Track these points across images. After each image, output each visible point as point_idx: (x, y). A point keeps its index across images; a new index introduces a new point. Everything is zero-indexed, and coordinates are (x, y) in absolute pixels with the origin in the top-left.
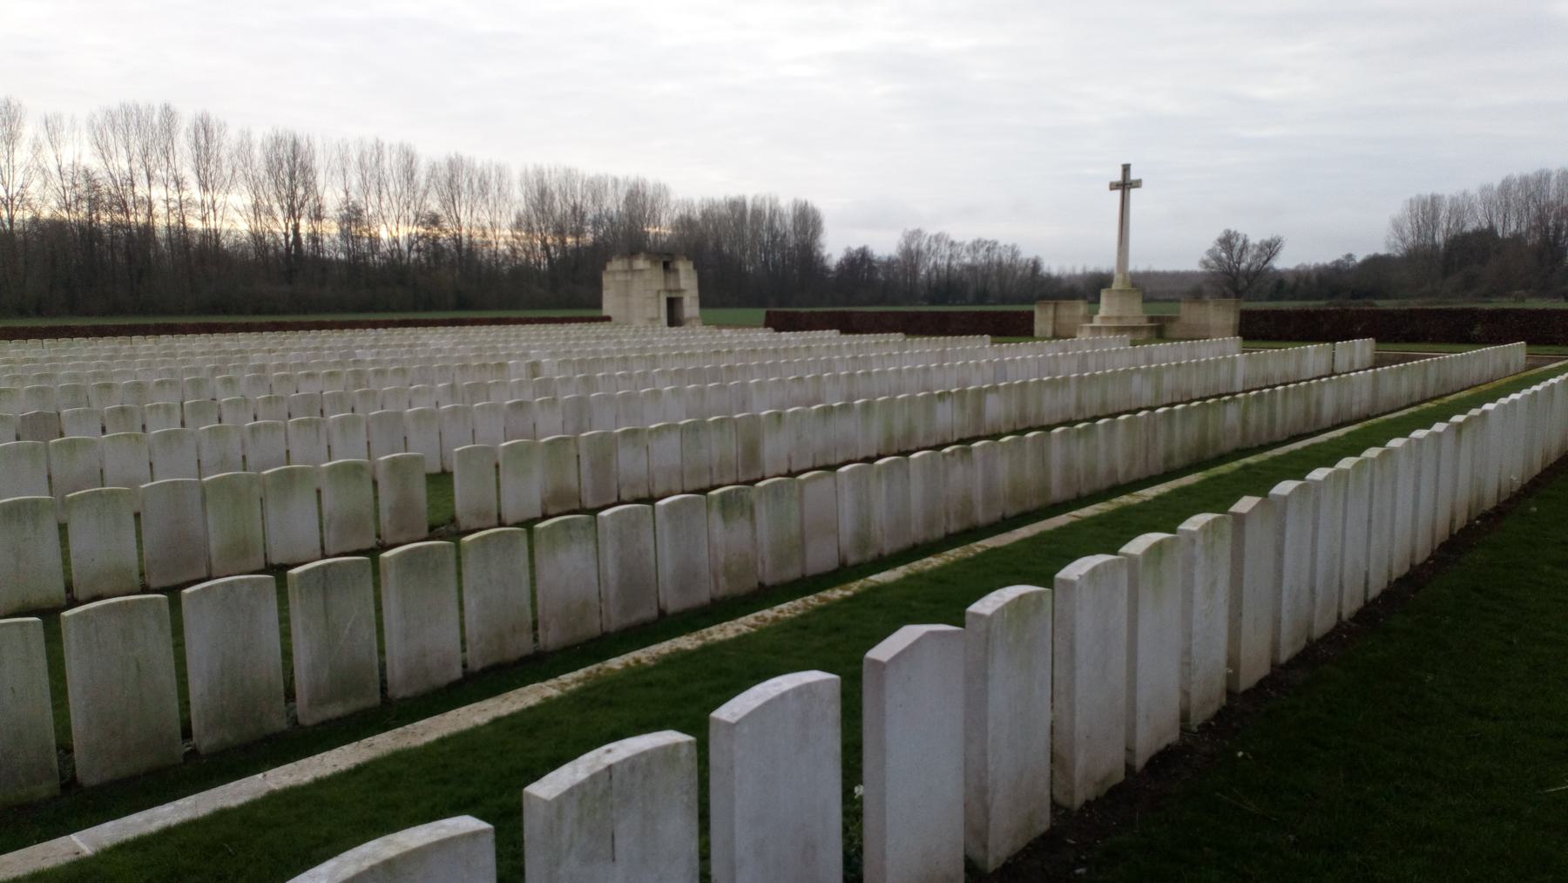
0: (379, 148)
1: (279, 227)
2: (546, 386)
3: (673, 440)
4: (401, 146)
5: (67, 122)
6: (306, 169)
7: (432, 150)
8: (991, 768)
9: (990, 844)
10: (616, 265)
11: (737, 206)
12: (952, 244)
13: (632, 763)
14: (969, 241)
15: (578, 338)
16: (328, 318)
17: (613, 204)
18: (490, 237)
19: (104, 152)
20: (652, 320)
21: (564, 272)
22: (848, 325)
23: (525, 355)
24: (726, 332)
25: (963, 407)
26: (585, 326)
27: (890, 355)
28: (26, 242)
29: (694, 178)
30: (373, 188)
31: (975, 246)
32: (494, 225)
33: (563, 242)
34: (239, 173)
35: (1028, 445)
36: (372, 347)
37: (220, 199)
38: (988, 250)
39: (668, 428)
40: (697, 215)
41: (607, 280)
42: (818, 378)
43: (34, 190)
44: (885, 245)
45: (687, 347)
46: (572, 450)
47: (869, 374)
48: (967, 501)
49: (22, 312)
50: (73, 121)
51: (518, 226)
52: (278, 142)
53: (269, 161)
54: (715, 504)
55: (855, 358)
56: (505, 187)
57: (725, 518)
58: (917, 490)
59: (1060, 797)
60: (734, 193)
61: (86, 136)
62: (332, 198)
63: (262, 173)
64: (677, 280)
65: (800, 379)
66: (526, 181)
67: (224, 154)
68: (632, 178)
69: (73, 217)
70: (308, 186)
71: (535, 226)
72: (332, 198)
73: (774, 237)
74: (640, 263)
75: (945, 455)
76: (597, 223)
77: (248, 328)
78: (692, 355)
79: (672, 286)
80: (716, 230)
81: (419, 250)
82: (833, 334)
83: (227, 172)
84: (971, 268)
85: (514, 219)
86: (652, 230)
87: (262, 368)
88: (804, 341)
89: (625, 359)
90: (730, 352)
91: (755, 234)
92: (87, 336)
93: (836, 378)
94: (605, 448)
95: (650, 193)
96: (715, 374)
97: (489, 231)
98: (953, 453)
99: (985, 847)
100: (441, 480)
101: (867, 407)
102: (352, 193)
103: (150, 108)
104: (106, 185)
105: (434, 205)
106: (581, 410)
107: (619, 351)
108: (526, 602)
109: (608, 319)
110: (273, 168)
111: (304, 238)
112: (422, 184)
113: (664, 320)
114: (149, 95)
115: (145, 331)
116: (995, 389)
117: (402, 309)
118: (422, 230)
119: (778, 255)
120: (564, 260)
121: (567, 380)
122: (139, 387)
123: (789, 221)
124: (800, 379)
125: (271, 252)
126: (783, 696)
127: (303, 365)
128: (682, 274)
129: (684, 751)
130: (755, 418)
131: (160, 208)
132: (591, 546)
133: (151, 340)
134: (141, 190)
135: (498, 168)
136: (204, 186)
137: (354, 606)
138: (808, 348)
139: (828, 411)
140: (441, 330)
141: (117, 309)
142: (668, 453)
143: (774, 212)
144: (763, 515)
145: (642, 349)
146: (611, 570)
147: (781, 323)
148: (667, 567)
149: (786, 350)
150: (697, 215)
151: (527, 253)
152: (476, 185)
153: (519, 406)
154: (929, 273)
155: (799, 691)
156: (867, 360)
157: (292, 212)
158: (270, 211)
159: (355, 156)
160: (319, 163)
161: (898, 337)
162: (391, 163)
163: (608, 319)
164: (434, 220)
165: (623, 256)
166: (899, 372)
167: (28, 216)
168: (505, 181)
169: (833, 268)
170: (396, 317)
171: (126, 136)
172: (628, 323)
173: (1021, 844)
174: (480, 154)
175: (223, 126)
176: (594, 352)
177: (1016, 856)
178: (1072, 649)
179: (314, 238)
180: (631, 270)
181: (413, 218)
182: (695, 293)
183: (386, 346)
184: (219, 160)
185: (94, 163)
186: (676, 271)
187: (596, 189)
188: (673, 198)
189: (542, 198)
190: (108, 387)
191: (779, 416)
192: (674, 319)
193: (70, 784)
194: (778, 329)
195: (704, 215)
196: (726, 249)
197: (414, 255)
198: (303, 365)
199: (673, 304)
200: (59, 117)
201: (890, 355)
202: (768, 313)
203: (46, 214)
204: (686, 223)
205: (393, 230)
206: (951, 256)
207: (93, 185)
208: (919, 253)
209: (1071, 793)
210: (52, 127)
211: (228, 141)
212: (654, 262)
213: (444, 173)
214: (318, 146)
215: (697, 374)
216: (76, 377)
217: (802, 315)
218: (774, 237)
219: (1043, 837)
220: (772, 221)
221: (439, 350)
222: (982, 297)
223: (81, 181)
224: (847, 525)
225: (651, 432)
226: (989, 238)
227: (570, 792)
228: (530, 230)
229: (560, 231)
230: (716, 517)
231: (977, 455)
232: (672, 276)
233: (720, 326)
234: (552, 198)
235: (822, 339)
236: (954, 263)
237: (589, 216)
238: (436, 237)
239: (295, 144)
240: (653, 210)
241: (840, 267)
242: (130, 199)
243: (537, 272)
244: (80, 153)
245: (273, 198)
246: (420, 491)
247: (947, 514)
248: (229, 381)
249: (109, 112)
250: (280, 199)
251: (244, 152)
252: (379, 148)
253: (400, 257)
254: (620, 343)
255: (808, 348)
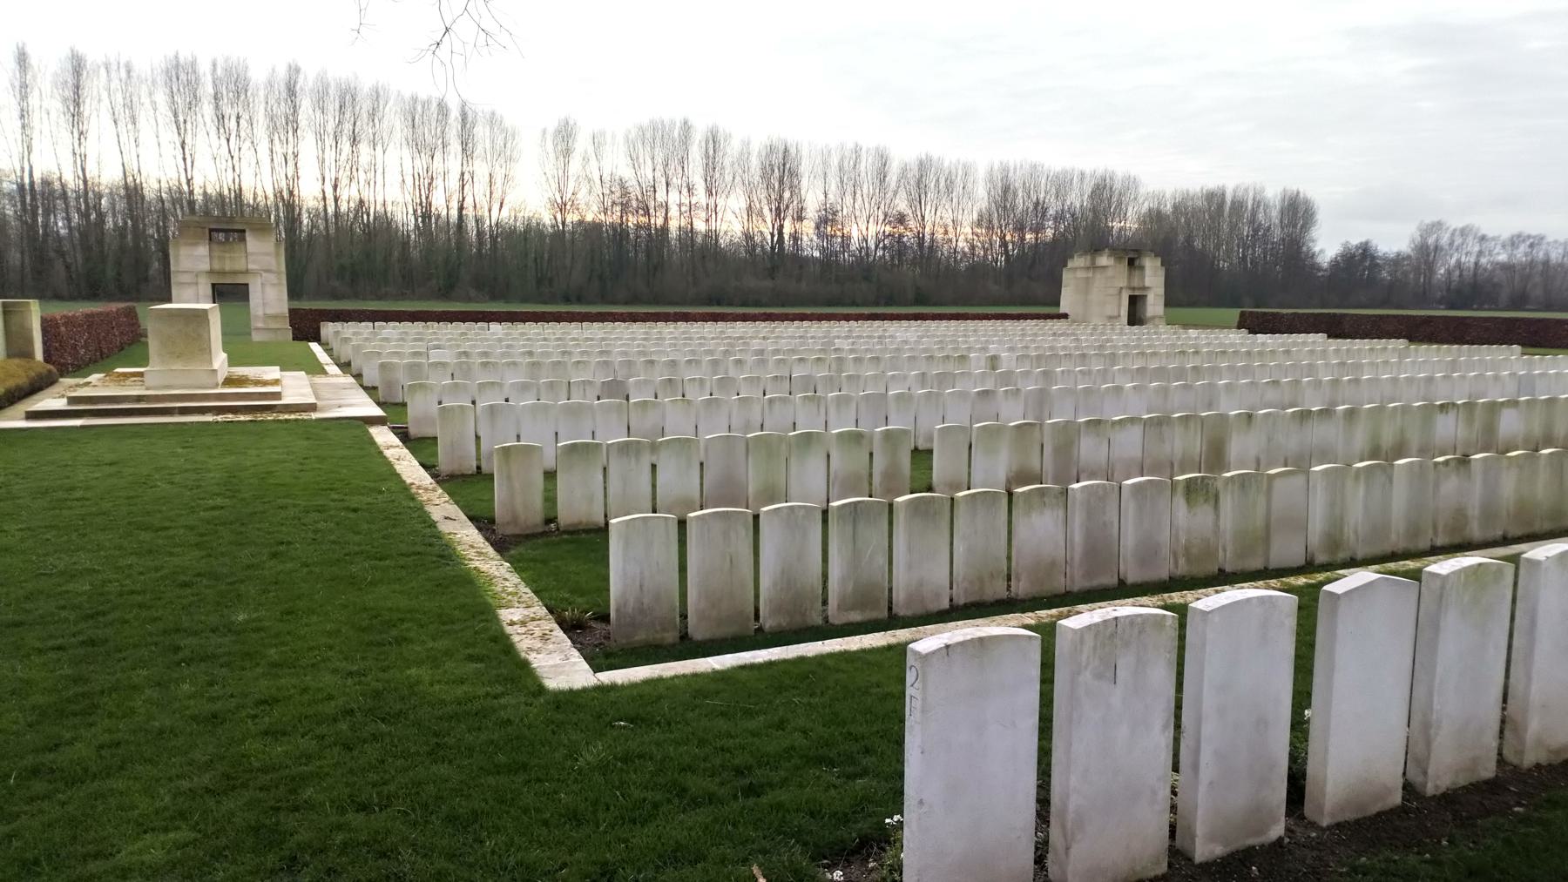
0: (857, 151)
1: (764, 228)
2: (1007, 377)
3: (1136, 432)
4: (877, 149)
5: (609, 139)
6: (793, 174)
7: (904, 154)
8: (1436, 706)
9: (1430, 771)
10: (1078, 262)
11: (1215, 199)
12: (1483, 238)
13: (1132, 619)
14: (1506, 235)
15: (1035, 335)
16: (808, 311)
17: (1077, 199)
18: (951, 235)
19: (634, 161)
20: (1110, 318)
21: (1023, 269)
22: (1336, 328)
23: (985, 349)
24: (1193, 333)
25: (1470, 421)
26: (1041, 322)
27: (1386, 362)
28: (573, 240)
29: (1164, 169)
30: (849, 189)
31: (1514, 242)
32: (957, 225)
33: (1022, 239)
34: (738, 178)
35: (1542, 462)
36: (847, 337)
37: (721, 202)
38: (1531, 246)
39: (1132, 420)
40: (1168, 208)
41: (1067, 276)
42: (1297, 382)
43: (582, 196)
44: (1393, 240)
45: (1149, 346)
46: (1037, 433)
47: (1357, 381)
48: (1460, 515)
49: (567, 300)
50: (613, 137)
51: (979, 223)
52: (772, 149)
53: (764, 168)
54: (1180, 489)
55: (1343, 364)
56: (970, 185)
57: (1188, 501)
58: (1399, 499)
59: (1509, 754)
60: (1211, 183)
61: (623, 148)
62: (813, 203)
63: (757, 178)
64: (1143, 278)
65: (1275, 383)
66: (990, 179)
67: (727, 162)
68: (1100, 171)
69: (609, 220)
70: (794, 189)
71: (995, 222)
72: (813, 203)
73: (1256, 231)
74: (1104, 260)
75: (1436, 464)
76: (1058, 218)
77: (744, 318)
78: (1154, 354)
79: (1136, 283)
80: (1188, 223)
81: (884, 248)
82: (1320, 338)
83: (728, 178)
84: (1507, 268)
85: (975, 216)
86: (1116, 225)
87: (761, 352)
88: (1283, 345)
89: (1084, 356)
90: (1196, 352)
91: (1234, 227)
92: (624, 321)
93: (1318, 384)
94: (1068, 436)
95: (1117, 186)
96: (1180, 373)
97: (950, 229)
98: (1446, 463)
99: (1425, 773)
100: (922, 456)
101: (1351, 414)
102: (830, 196)
103: (673, 123)
104: (635, 192)
105: (902, 205)
106: (1042, 399)
107: (1077, 348)
108: (1004, 555)
109: (1065, 316)
110: (766, 174)
111: (786, 237)
112: (893, 185)
113: (1125, 319)
114: (671, 113)
115: (666, 318)
116: (1514, 403)
117: (865, 304)
118: (888, 229)
119: (1259, 251)
120: (1022, 255)
121: (1026, 374)
122: (673, 363)
123: (1275, 213)
124: (1275, 383)
125: (758, 250)
126: (1249, 600)
127: (793, 351)
128: (1148, 271)
129: (1169, 622)
130: (1223, 418)
131: (674, 212)
132: (1061, 513)
133: (671, 325)
134: (661, 196)
135: (965, 166)
136: (709, 192)
137: (874, 536)
138: (1288, 352)
139: (1305, 415)
140: (905, 323)
141: (634, 300)
142: (1129, 443)
143: (1257, 203)
144: (1227, 503)
145: (1101, 347)
146: (1078, 538)
147: (1255, 324)
148: (1129, 541)
149: (1260, 353)
150: (1168, 208)
151: (986, 250)
152: (942, 184)
153: (985, 394)
154: (1449, 272)
155: (1261, 599)
156: (1358, 367)
157: (778, 214)
158: (761, 214)
159: (835, 161)
160: (804, 169)
161: (1401, 343)
162: (867, 165)
163: (1065, 316)
164: (901, 219)
165: (1086, 252)
166: (1395, 380)
167: (576, 218)
168: (971, 179)
169: (1325, 265)
170: (866, 311)
171: (652, 148)
172: (1084, 320)
173: (1463, 781)
174: (948, 151)
175: (728, 137)
176: (1052, 348)
177: (1455, 790)
178: (1533, 623)
179: (795, 237)
180: (1093, 267)
181: (881, 217)
182: (1161, 291)
183: (859, 337)
184: (723, 168)
185: (627, 173)
186: (1142, 268)
187: (1061, 185)
188: (1142, 191)
189: (1004, 194)
190: (652, 362)
191: (1250, 416)
192: (1135, 318)
193: (684, 636)
194: (1253, 331)
195: (1176, 207)
196: (1198, 244)
197: (879, 253)
198: (793, 351)
199: (1134, 301)
200: (603, 134)
201: (1386, 362)
202: (1242, 314)
203: (589, 218)
204: (1155, 216)
205: (863, 229)
206: (1480, 253)
207: (625, 193)
208: (1437, 248)
209: (1521, 753)
210: (597, 141)
211: (731, 150)
212: (1119, 259)
213: (913, 173)
214: (805, 153)
215: (1161, 373)
216: (626, 353)
217: (1283, 316)
218: (1256, 231)
219: (1487, 782)
220: (1254, 213)
221: (906, 342)
222: (1519, 301)
223: (616, 188)
224: (1317, 525)
225: (1114, 423)
226: (1534, 233)
227: (1089, 627)
228: (990, 227)
229: (1020, 228)
230: (1180, 501)
231: (1476, 469)
232: (1137, 273)
233: (1186, 326)
234: (1015, 194)
235: (1304, 343)
236: (1483, 261)
237: (1051, 212)
238: (901, 236)
239: (786, 151)
240: (1120, 203)
241: (1335, 264)
242: (651, 205)
243: (994, 269)
244: (618, 165)
245: (764, 201)
246: (906, 461)
247: (1435, 527)
248: (739, 362)
249: (641, 128)
250: (769, 203)
251: (744, 156)
252: (857, 151)
253: (867, 254)
254: (1077, 340)
255: (1288, 352)
